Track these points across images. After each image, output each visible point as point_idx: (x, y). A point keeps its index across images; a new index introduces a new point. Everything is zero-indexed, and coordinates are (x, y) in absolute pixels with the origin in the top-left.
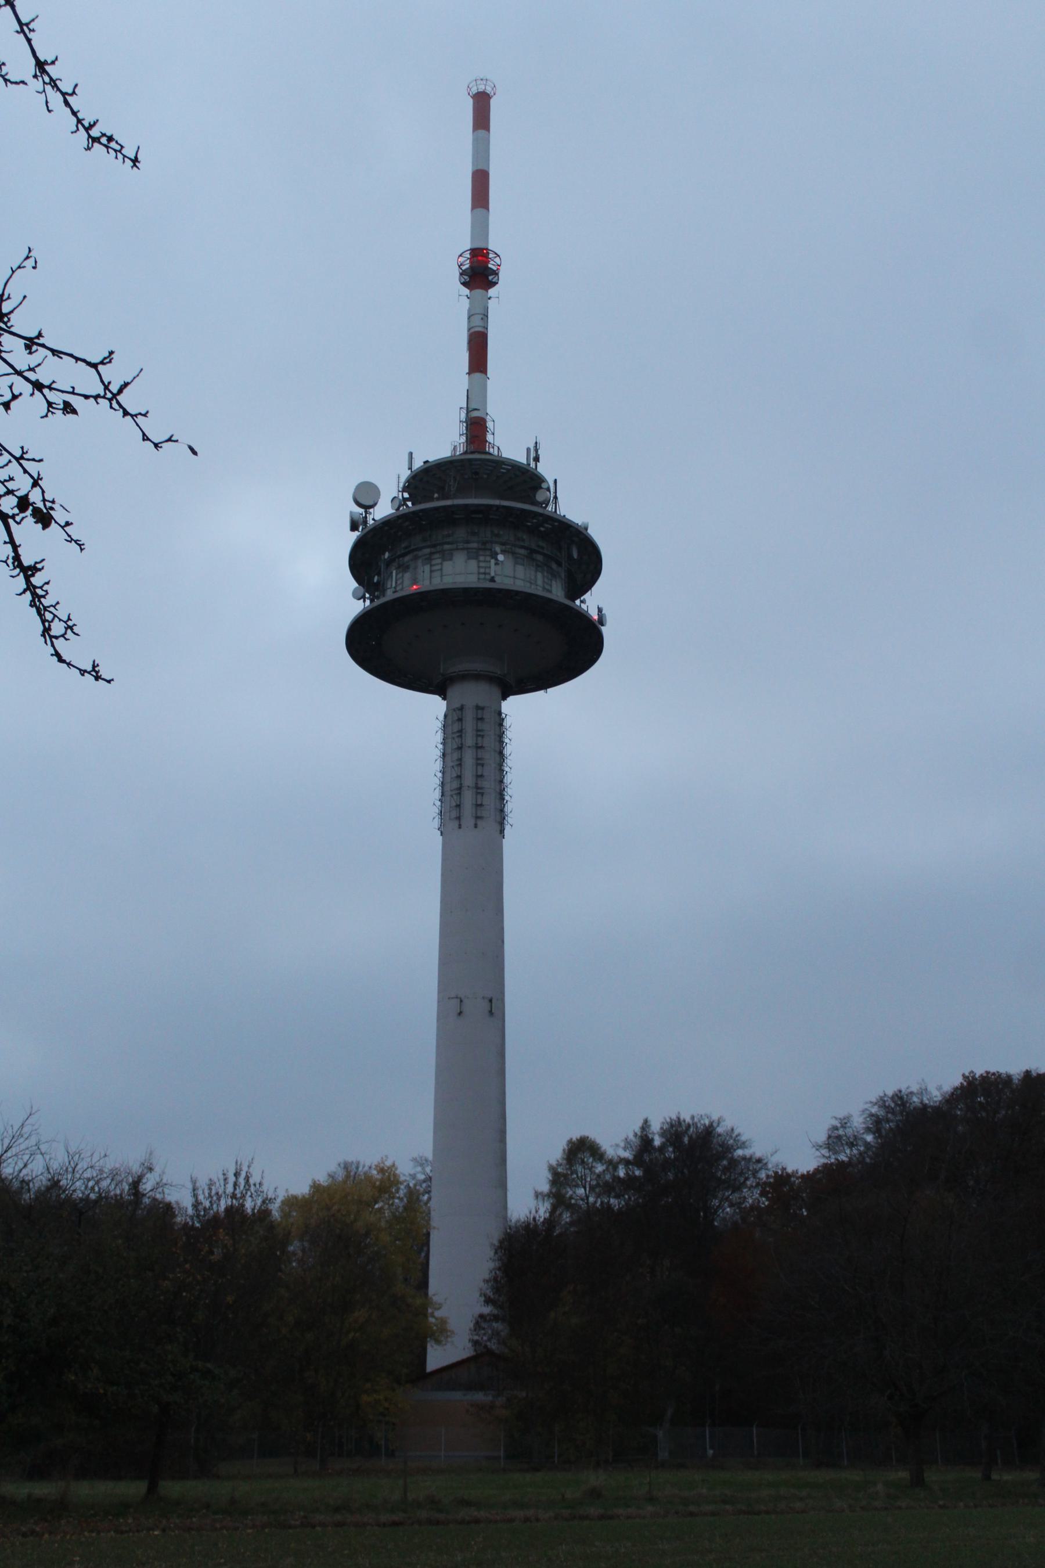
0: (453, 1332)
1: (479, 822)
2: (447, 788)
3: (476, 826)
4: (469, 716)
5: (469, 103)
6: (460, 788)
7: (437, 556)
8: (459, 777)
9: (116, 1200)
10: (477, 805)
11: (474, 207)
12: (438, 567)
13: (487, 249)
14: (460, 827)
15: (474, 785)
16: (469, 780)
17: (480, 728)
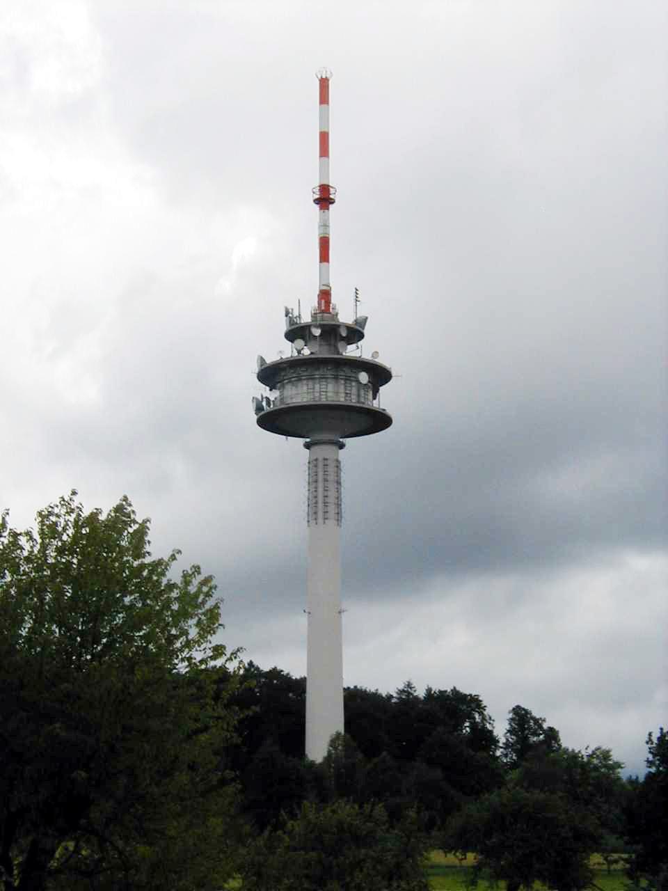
1: (326, 521)
3: (324, 523)
4: (320, 464)
5: (318, 83)
7: (324, 380)
9: (246, 670)
10: (325, 512)
11: (321, 262)
13: (328, 186)
15: (324, 496)
17: (326, 500)
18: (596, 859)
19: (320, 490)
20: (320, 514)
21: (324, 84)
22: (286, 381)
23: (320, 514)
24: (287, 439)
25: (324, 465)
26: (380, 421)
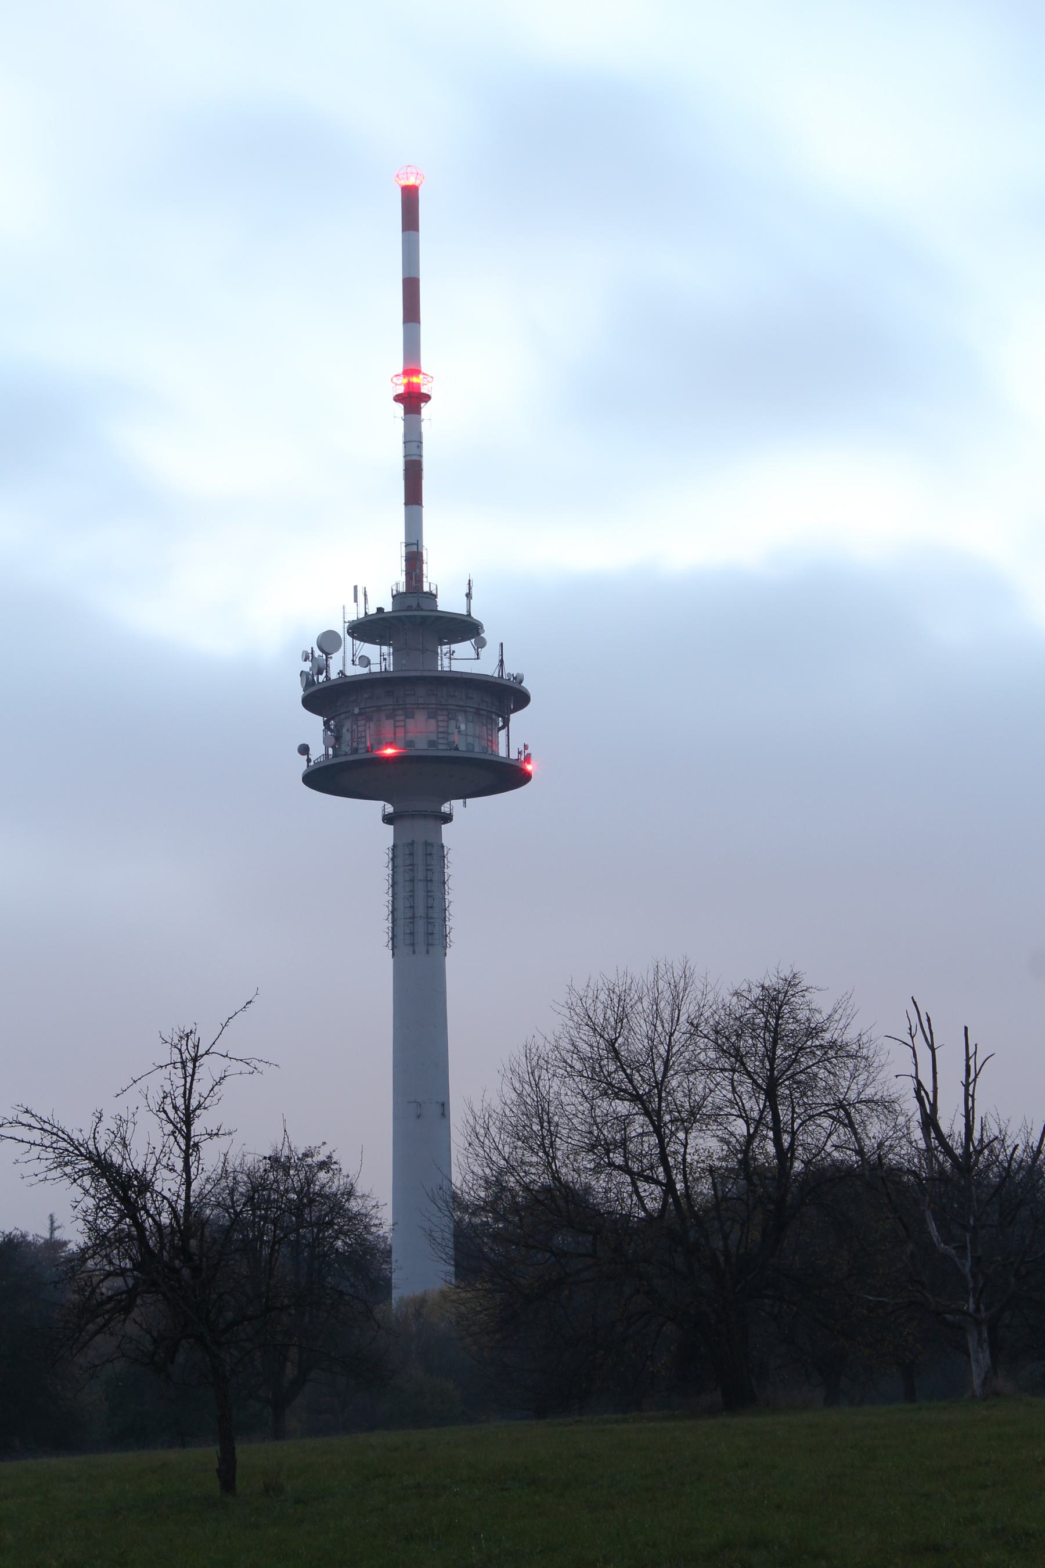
0: (425, 1292)
1: (430, 948)
2: (400, 914)
3: (428, 952)
6: (413, 917)
8: (412, 907)
12: (402, 724)
14: (414, 952)
16: (420, 911)
18: (165, 1219)
19: (420, 894)
20: (420, 937)
21: (410, 197)
22: (343, 716)
23: (420, 937)
24: (465, 803)
25: (427, 855)
26: (510, 776)
